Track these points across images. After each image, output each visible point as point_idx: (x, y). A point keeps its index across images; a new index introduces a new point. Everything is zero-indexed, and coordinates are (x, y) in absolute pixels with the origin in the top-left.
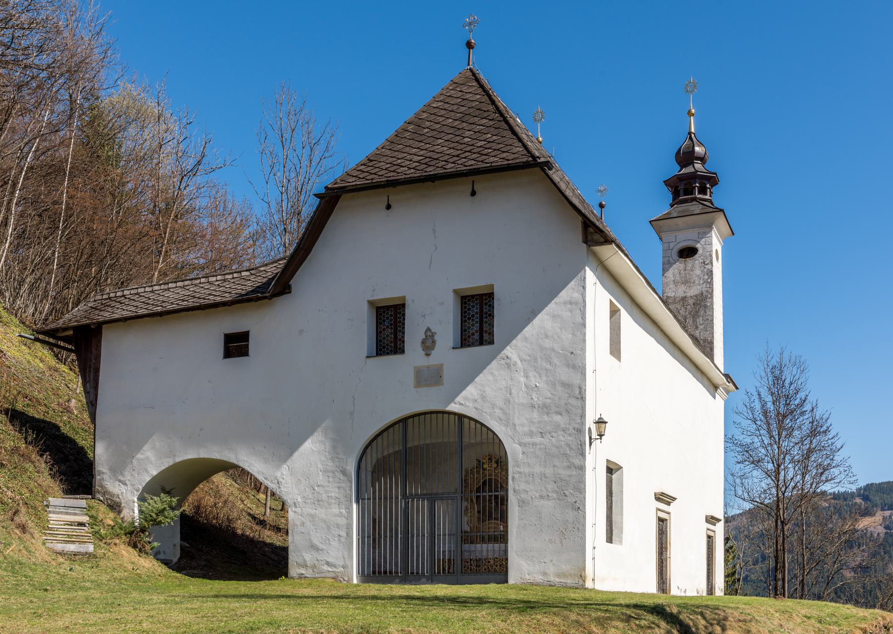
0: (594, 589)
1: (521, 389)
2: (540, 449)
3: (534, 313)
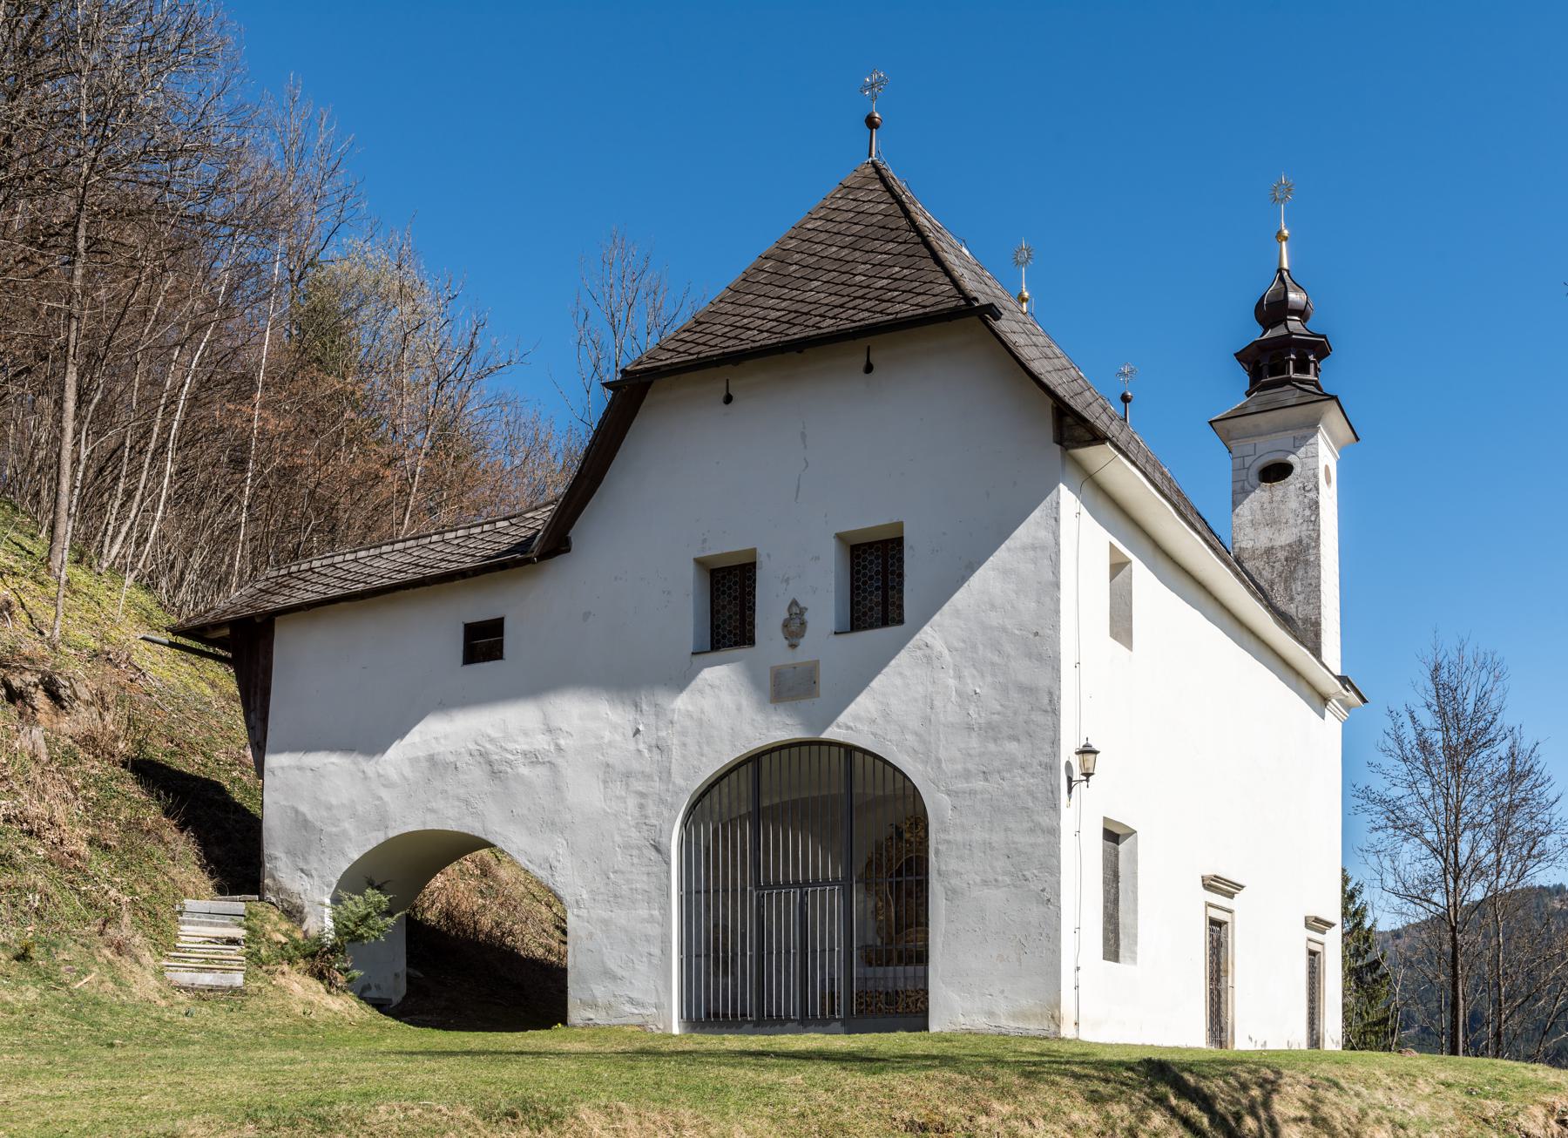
0: (1078, 1039)
1: (949, 699)
3: (971, 568)
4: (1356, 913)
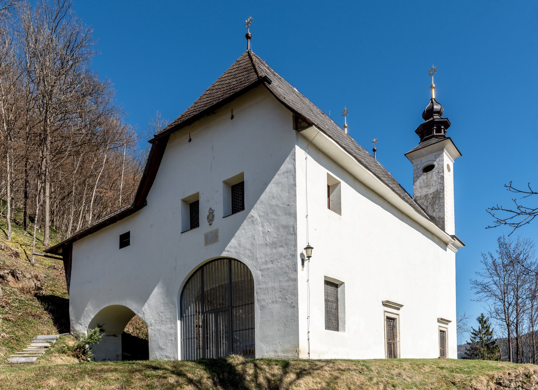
1: (260, 235)
2: (271, 271)
3: (266, 184)
4: (486, 327)
